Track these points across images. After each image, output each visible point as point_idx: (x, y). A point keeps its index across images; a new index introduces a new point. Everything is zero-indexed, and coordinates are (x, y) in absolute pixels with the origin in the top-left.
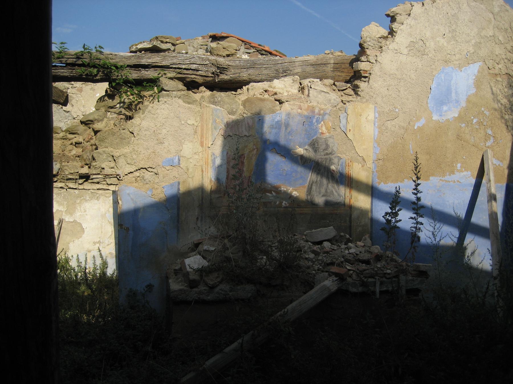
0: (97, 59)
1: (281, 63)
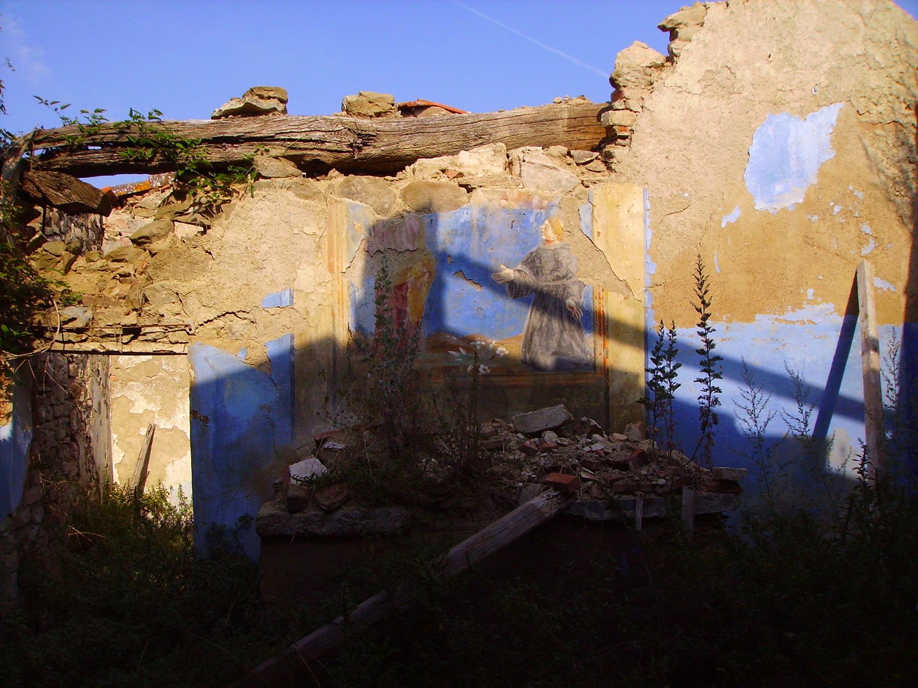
0: (153, 132)
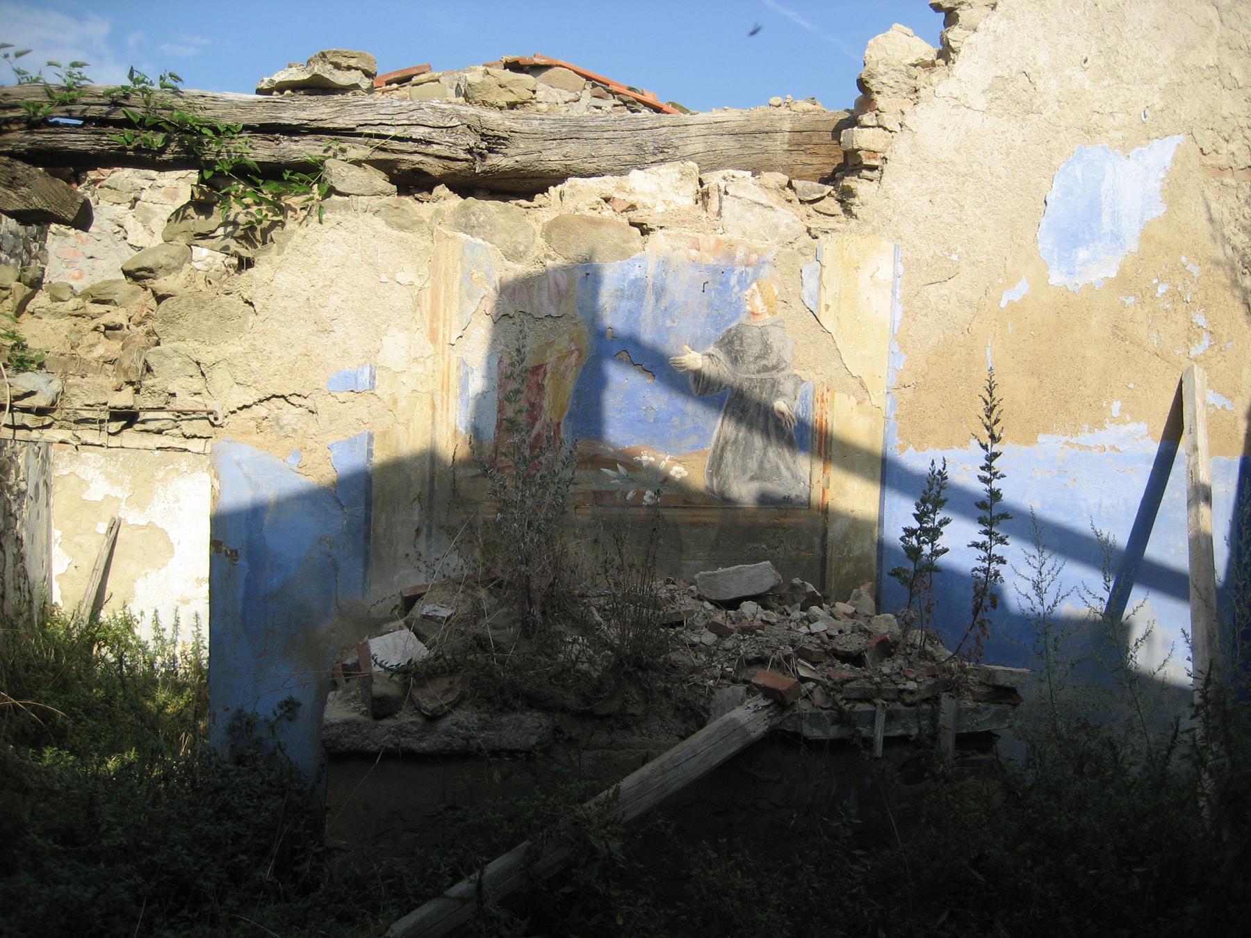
0: (165, 108)
1: (651, 128)
